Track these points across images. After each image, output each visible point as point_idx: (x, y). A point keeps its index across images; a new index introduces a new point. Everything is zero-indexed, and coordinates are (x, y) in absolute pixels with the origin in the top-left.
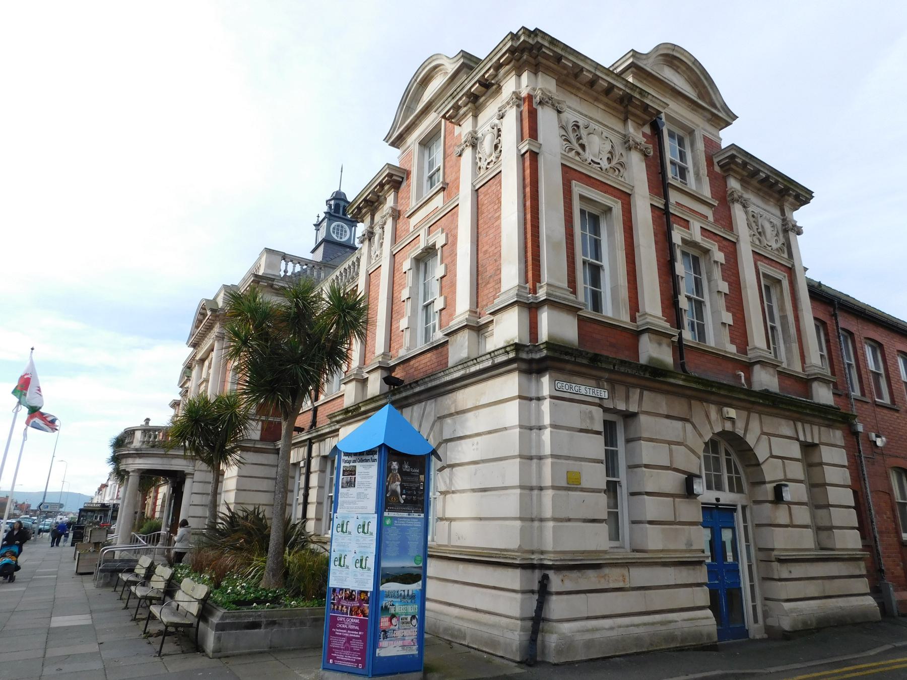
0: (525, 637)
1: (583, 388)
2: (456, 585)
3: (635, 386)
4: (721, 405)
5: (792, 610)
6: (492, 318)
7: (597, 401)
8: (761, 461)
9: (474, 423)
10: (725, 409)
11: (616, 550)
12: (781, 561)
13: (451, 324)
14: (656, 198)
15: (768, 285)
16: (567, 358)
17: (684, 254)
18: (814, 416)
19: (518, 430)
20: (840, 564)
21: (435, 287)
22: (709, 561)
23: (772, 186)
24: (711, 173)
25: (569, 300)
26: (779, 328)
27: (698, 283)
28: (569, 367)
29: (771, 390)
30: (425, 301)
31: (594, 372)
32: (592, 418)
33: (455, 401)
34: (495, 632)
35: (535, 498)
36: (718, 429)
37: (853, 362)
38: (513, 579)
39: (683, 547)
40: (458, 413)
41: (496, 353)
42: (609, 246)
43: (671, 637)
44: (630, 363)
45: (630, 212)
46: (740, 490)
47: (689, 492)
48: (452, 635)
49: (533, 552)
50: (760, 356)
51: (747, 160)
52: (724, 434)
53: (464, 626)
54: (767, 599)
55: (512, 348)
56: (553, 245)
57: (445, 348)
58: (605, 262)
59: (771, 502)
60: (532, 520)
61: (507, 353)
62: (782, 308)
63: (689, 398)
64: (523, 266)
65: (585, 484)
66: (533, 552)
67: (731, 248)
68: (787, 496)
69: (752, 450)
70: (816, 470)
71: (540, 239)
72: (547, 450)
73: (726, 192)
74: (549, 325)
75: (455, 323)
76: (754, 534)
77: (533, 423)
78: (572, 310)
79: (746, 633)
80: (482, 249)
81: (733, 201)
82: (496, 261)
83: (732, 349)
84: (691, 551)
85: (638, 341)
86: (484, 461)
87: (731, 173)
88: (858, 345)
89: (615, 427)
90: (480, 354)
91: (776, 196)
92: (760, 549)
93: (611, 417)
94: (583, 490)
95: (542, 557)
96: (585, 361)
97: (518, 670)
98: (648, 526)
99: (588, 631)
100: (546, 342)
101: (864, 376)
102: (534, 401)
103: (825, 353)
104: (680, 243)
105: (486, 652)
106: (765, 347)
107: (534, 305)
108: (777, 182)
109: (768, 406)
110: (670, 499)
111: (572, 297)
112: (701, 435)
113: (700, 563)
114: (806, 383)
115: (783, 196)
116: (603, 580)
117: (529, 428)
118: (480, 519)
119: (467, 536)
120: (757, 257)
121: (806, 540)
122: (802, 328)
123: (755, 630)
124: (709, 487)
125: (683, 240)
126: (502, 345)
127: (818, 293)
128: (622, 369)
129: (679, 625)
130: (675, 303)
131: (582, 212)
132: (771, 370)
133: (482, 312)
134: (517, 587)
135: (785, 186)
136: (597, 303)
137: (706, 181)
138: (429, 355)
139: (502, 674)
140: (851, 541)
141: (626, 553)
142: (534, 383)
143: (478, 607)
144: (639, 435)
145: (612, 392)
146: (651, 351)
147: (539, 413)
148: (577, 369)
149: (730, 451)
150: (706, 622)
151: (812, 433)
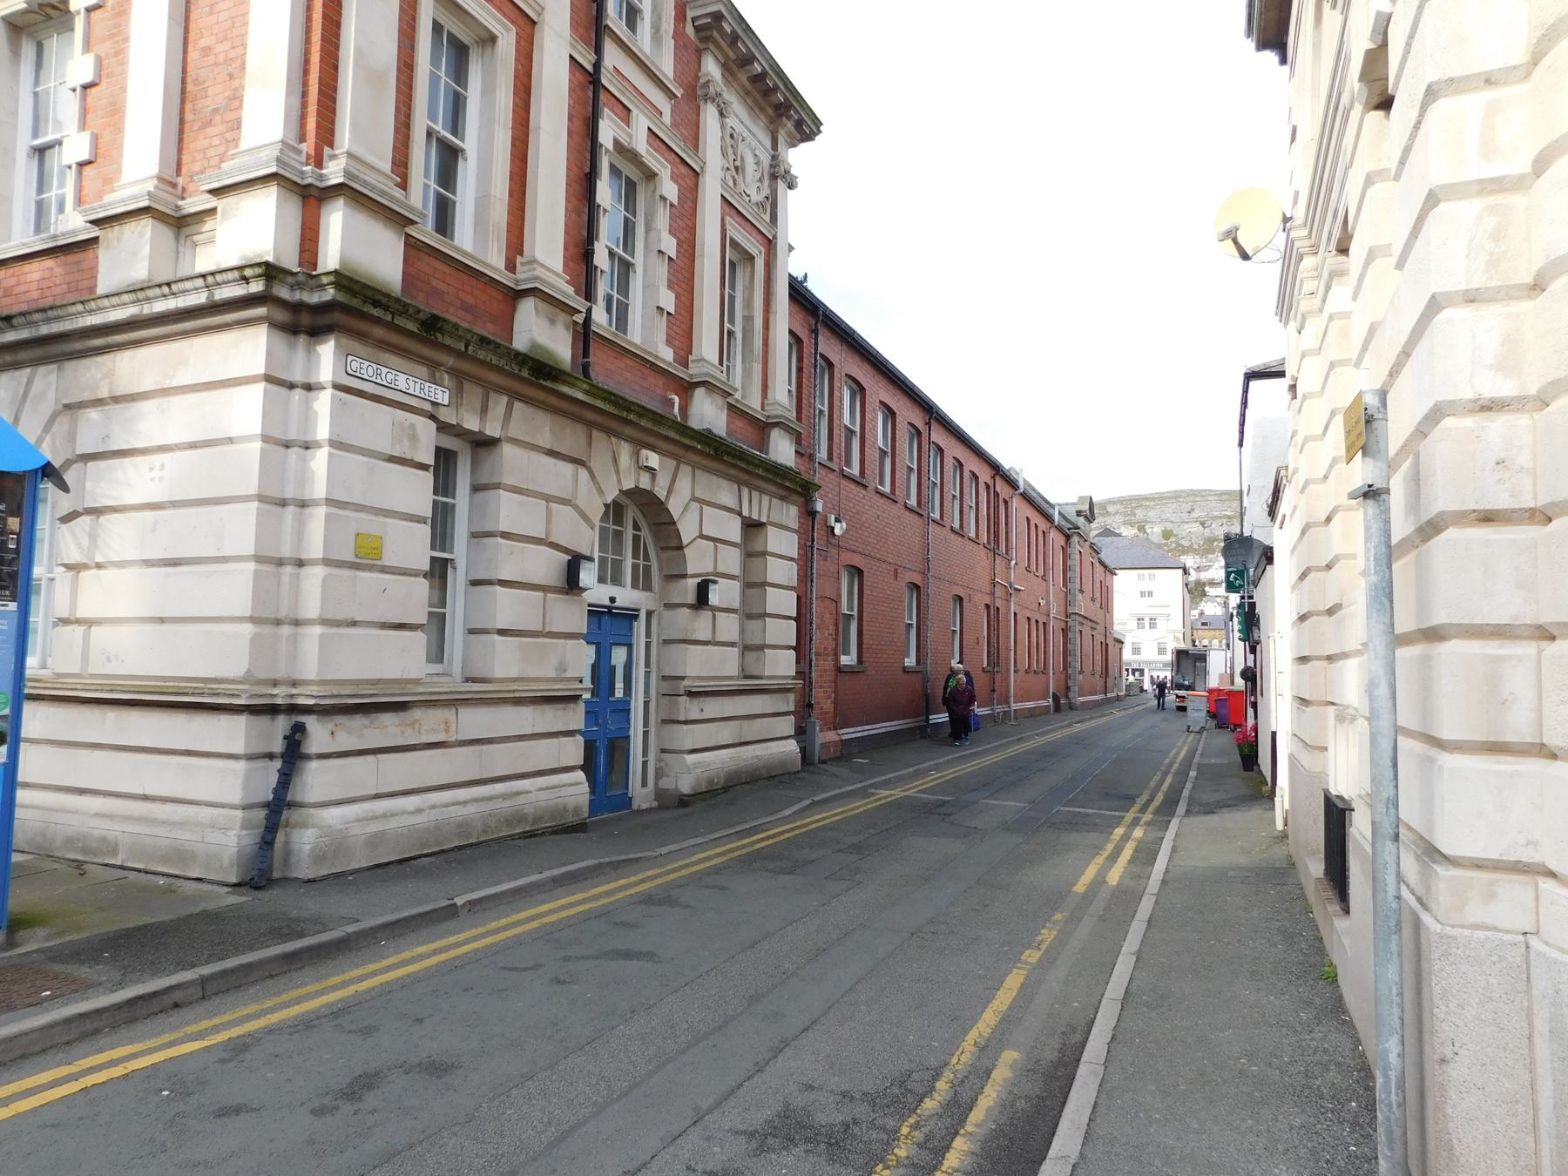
0: (250, 839)
1: (402, 377)
2: (98, 753)
3: (500, 390)
4: (639, 444)
5: (696, 765)
6: (211, 202)
7: (427, 407)
8: (685, 542)
9: (152, 424)
10: (644, 452)
11: (436, 679)
12: (691, 694)
13: (108, 198)
14: (581, 47)
15: (736, 261)
16: (376, 312)
17: (614, 170)
18: (765, 479)
19: (258, 445)
20: (765, 697)
21: (66, 108)
22: (587, 696)
23: (768, 92)
24: (678, 34)
25: (392, 198)
26: (739, 336)
27: (629, 229)
28: (378, 332)
29: (715, 431)
30: (35, 135)
31: (426, 351)
32: (413, 438)
33: (111, 373)
34: (185, 835)
35: (286, 579)
36: (628, 484)
37: (826, 409)
38: (232, 733)
39: (552, 674)
40: (116, 399)
41: (219, 278)
42: (482, 114)
43: (520, 817)
44: (498, 346)
45: (531, 43)
46: (648, 587)
47: (571, 584)
48: (85, 851)
49: (275, 684)
50: (708, 374)
51: (740, 32)
52: (636, 494)
53: (113, 829)
54: (664, 751)
55: (259, 271)
56: (370, 76)
57: (90, 254)
58: (470, 143)
59: (691, 606)
60: (278, 622)
61: (246, 280)
62: (748, 305)
63: (591, 425)
64: (296, 102)
65: (389, 559)
66: (275, 684)
67: (691, 178)
68: (714, 598)
69: (674, 523)
70: (757, 561)
71: (341, 53)
72: (319, 490)
73: (697, 78)
74: (343, 239)
75: (116, 201)
76: (659, 655)
77: (293, 435)
78: (398, 220)
79: (626, 801)
80: (198, 43)
81: (706, 98)
82: (231, 76)
83: (666, 354)
84: (562, 680)
85: (514, 309)
86: (175, 504)
87: (712, 47)
88: (837, 384)
89: (456, 459)
90: (180, 275)
91: (770, 111)
92: (665, 678)
93: (450, 443)
94: (385, 570)
95: (294, 691)
96: (412, 326)
97: (234, 899)
98: (496, 637)
99: (375, 818)
100: (336, 272)
101: (836, 431)
102: (298, 391)
103: (794, 388)
104: (611, 147)
105: (163, 875)
106: (716, 362)
107: (313, 192)
108: (776, 88)
109: (707, 455)
110: (540, 594)
111: (398, 193)
112: (600, 491)
113: (575, 699)
114: (763, 428)
115: (780, 116)
116: (409, 731)
117: (284, 443)
118: (162, 620)
119: (131, 655)
120: (727, 209)
121: (727, 664)
122: (771, 342)
123: (641, 794)
124: (601, 580)
125: (616, 142)
126: (235, 262)
127: (799, 294)
128: (481, 355)
129: (532, 797)
130: (587, 255)
131: (437, 28)
132: (720, 400)
133: (191, 187)
134: (239, 749)
135: (786, 99)
136: (444, 221)
137: (669, 44)
138: (49, 263)
139: (198, 910)
140: (782, 665)
141: (454, 684)
142: (300, 353)
143: (148, 792)
144: (496, 480)
145: (458, 394)
146: (534, 330)
147: (308, 416)
148: (394, 338)
149: (643, 520)
150: (575, 790)
151: (761, 506)
